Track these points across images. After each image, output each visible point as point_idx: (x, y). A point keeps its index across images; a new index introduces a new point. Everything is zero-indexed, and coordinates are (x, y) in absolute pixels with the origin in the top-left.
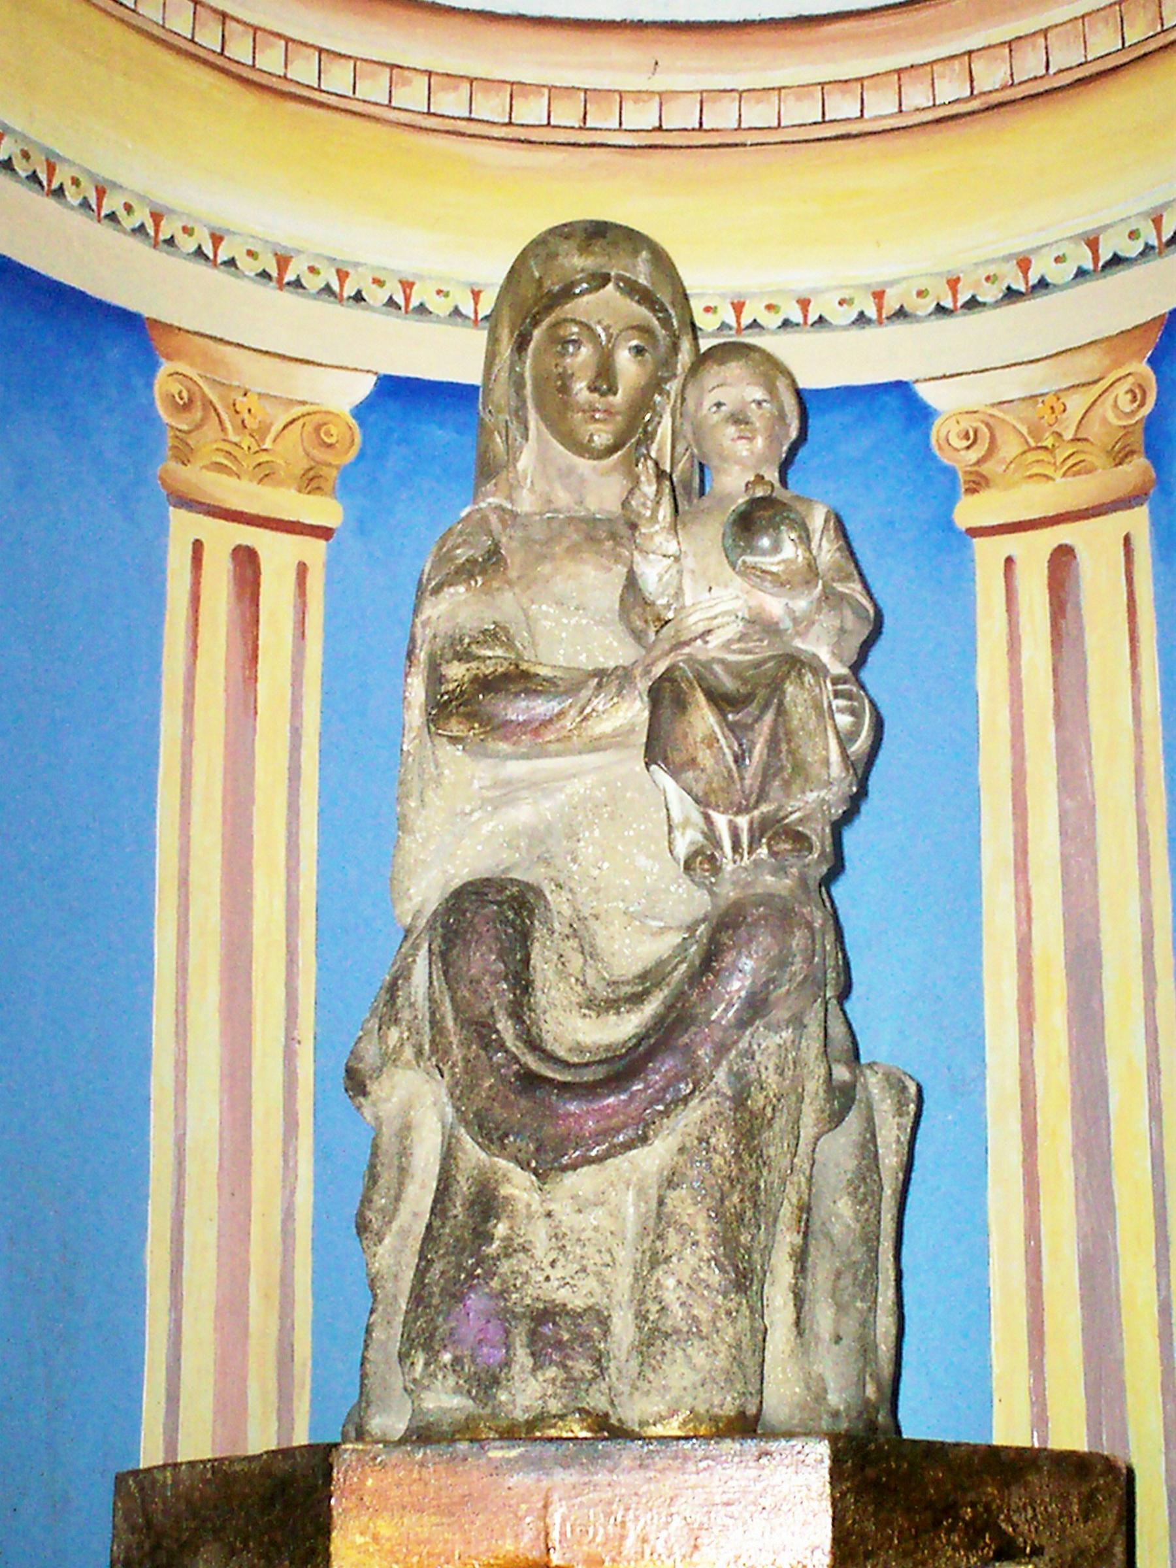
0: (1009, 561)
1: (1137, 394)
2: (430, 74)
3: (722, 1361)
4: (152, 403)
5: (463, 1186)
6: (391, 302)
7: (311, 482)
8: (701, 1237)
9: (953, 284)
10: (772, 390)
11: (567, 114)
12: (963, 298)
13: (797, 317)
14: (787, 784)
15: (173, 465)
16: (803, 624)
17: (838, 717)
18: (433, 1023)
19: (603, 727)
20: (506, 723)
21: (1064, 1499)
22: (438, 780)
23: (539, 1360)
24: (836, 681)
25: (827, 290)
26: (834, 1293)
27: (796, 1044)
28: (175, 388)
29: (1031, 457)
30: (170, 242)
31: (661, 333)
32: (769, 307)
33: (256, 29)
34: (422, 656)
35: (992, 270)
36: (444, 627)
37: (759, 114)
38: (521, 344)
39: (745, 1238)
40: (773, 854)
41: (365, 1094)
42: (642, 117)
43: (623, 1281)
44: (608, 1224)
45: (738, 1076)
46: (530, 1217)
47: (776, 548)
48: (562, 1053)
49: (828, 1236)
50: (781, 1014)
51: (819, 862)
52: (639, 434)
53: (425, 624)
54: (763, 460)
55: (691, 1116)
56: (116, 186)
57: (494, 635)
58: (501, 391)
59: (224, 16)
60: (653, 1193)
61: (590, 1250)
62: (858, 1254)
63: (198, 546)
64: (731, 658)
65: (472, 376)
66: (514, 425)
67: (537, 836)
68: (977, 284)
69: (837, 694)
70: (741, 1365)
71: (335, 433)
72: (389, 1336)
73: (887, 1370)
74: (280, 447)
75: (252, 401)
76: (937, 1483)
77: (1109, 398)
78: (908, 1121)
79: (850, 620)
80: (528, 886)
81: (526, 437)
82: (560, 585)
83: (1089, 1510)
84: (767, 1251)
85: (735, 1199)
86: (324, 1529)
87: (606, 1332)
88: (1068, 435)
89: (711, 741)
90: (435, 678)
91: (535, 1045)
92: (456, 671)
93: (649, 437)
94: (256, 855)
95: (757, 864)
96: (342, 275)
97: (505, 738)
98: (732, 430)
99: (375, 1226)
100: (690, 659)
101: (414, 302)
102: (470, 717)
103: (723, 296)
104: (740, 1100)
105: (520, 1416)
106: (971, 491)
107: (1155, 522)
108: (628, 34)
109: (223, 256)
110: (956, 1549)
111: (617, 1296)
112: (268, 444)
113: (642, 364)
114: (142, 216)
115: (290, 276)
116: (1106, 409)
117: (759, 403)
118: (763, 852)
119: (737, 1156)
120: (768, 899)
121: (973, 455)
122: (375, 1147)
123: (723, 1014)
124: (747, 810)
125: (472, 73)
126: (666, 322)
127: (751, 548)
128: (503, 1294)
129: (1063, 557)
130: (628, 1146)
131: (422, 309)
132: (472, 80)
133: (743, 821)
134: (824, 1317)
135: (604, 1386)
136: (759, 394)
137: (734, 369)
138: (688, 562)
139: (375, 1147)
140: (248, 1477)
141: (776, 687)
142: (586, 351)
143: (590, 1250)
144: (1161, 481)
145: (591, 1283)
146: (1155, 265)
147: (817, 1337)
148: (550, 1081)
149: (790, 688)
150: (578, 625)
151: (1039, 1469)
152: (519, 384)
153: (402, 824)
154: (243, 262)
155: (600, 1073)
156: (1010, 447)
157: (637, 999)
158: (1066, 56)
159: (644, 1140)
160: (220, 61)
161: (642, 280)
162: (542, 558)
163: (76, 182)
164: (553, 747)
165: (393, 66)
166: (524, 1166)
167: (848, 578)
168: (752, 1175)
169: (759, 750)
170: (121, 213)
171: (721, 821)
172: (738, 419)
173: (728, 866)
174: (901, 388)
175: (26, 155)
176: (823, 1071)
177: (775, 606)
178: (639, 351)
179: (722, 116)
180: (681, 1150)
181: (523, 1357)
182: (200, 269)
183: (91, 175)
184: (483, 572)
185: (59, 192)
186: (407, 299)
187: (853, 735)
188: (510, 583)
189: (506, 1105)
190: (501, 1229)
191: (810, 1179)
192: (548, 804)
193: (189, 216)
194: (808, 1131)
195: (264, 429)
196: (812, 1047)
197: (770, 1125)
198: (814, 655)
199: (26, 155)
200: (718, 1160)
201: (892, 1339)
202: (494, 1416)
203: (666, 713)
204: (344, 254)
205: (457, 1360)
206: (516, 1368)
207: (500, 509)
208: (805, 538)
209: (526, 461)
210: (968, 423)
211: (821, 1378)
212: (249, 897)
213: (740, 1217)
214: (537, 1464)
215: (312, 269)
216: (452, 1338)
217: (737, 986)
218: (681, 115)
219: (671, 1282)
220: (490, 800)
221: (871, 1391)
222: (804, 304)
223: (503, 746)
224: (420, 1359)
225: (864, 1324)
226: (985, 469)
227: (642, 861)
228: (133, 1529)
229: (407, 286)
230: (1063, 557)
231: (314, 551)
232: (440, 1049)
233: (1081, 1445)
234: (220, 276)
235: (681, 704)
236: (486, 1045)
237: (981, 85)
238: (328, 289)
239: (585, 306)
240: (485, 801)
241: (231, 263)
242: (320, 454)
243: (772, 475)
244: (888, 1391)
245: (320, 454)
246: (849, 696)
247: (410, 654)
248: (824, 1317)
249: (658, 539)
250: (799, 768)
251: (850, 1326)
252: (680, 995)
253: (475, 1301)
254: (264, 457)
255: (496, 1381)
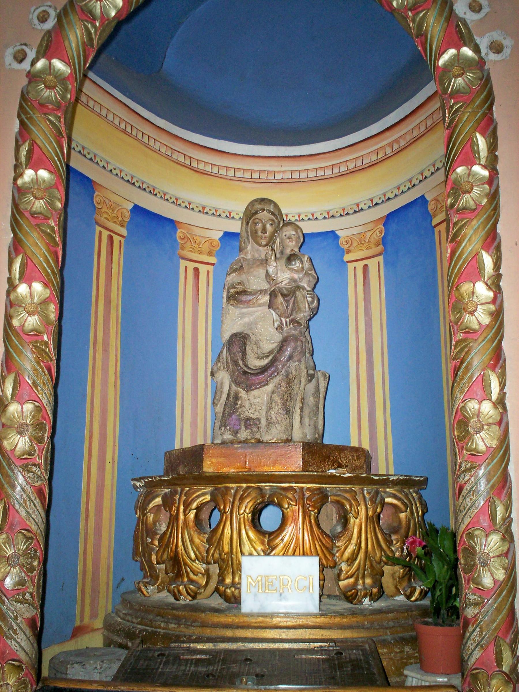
0: (355, 268)
1: (381, 232)
2: (235, 168)
3: (283, 428)
4: (176, 238)
5: (232, 394)
6: (227, 216)
7: (210, 254)
8: (279, 404)
9: (344, 210)
10: (297, 232)
11: (263, 176)
12: (345, 213)
13: (311, 217)
14: (296, 312)
15: (180, 250)
16: (301, 279)
17: (308, 299)
18: (226, 362)
19: (261, 301)
20: (241, 301)
21: (353, 456)
22: (229, 313)
23: (246, 428)
24: (307, 291)
25: (317, 212)
26: (309, 417)
27: (299, 365)
28: (181, 235)
29: (359, 246)
30: (180, 205)
31: (276, 221)
32: (306, 216)
33: (198, 160)
34: (226, 288)
35: (352, 206)
36: (231, 282)
37: (303, 175)
38: (247, 224)
39: (288, 404)
40: (294, 326)
41: (214, 376)
42: (279, 176)
43: (264, 413)
44: (261, 401)
45: (287, 371)
46: (245, 400)
47: (295, 264)
48: (252, 367)
49: (308, 404)
50: (296, 359)
51: (303, 328)
52: (272, 242)
53: (227, 281)
54: (295, 246)
55: (276, 380)
56: (168, 193)
57: (240, 284)
58: (244, 234)
59: (191, 158)
60: (270, 395)
61: (257, 407)
62: (314, 408)
63: (186, 267)
64: (287, 287)
65: (238, 231)
66: (246, 241)
67: (249, 324)
68: (348, 210)
69: (308, 294)
70: (287, 429)
71: (215, 244)
72: (218, 424)
73: (321, 432)
74: (203, 247)
75: (197, 237)
76: (325, 452)
77: (375, 233)
78: (327, 382)
79: (311, 279)
80: (247, 334)
81: (249, 243)
82: (255, 273)
83: (358, 458)
84: (294, 407)
85: (286, 396)
86: (202, 461)
87: (260, 423)
88: (367, 241)
89: (282, 303)
90: (228, 292)
91: (246, 366)
92: (232, 291)
93: (274, 243)
94: (199, 330)
95: (290, 328)
96: (216, 211)
97: (241, 304)
98: (288, 240)
99: (216, 403)
100: (278, 287)
101: (232, 216)
102: (235, 300)
103: (296, 213)
104: (287, 376)
105: (242, 439)
106: (347, 253)
107: (384, 258)
108: (276, 159)
109: (191, 207)
110: (329, 465)
111: (262, 415)
112: (201, 246)
113: (272, 227)
114: (174, 199)
115: (205, 211)
116: (374, 235)
117: (294, 235)
118: (292, 326)
119: (287, 388)
120: (293, 335)
121: (348, 246)
122: (216, 387)
123: (284, 358)
124: (289, 317)
125: (244, 168)
126: (277, 218)
127: (290, 264)
128: (239, 415)
129: (366, 267)
130: (264, 386)
131: (233, 218)
132: (243, 169)
133: (288, 320)
134: (307, 421)
135: (259, 433)
136: (294, 233)
137: (289, 228)
138: (279, 268)
139: (216, 387)
140: (188, 451)
141: (294, 292)
142: (260, 225)
143: (257, 407)
144: (385, 250)
145: (257, 413)
146: (384, 205)
147: (305, 425)
148: (249, 373)
149: (297, 293)
150: (258, 282)
151: (348, 450)
152: (247, 232)
153: (222, 322)
154: (195, 209)
155: (259, 371)
156: (355, 244)
157: (267, 356)
158: (366, 161)
159: (267, 384)
160: (190, 167)
161: (272, 210)
162: (251, 268)
163: (159, 193)
164: (251, 306)
165: (227, 167)
166: (243, 389)
167: (311, 270)
168: (290, 391)
169: (291, 305)
170: (169, 199)
171: (283, 320)
172: (289, 238)
173: (285, 329)
174: (333, 232)
175: (148, 187)
176: (306, 371)
177: (296, 276)
178: (271, 225)
179: (296, 176)
180: (275, 386)
181: (243, 428)
182: (186, 210)
183: (163, 191)
184: (239, 271)
185: (156, 195)
186: (230, 216)
187: (312, 302)
188: (245, 273)
189: (241, 378)
190: (239, 402)
191: (304, 393)
192: (251, 318)
193: (184, 199)
194: (303, 384)
195: (200, 243)
196: (303, 366)
197: (294, 381)
198: (304, 286)
199: (148, 187)
200: (283, 388)
201: (322, 426)
202: (237, 439)
203: (273, 298)
204: (204, 204)
205: (230, 428)
206: (242, 430)
207: (243, 258)
208: (302, 262)
209: (249, 248)
210: (346, 239)
211: (306, 433)
212: (197, 339)
213: (287, 400)
214: (244, 448)
215: (210, 210)
216: (229, 424)
217: (287, 353)
218: (287, 176)
219: (273, 413)
220: (239, 317)
221: (317, 436)
222: (313, 215)
223: (241, 306)
224: (223, 428)
225: (315, 422)
226: (350, 248)
227: (270, 329)
228: (168, 463)
229: (230, 213)
230: (366, 267)
231: (211, 268)
232: (228, 367)
233: (356, 445)
234: (191, 212)
235: (276, 296)
236: (236, 365)
237: (350, 167)
238: (213, 214)
239: (260, 215)
240: (239, 317)
241: (193, 209)
242: (212, 248)
243: (297, 250)
244: (321, 436)
245: (212, 248)
246: (311, 294)
247: (224, 287)
248: (307, 421)
249: (272, 263)
250: (299, 309)
251: (312, 423)
252: (275, 355)
253: (234, 417)
254: (200, 249)
255: (237, 432)
